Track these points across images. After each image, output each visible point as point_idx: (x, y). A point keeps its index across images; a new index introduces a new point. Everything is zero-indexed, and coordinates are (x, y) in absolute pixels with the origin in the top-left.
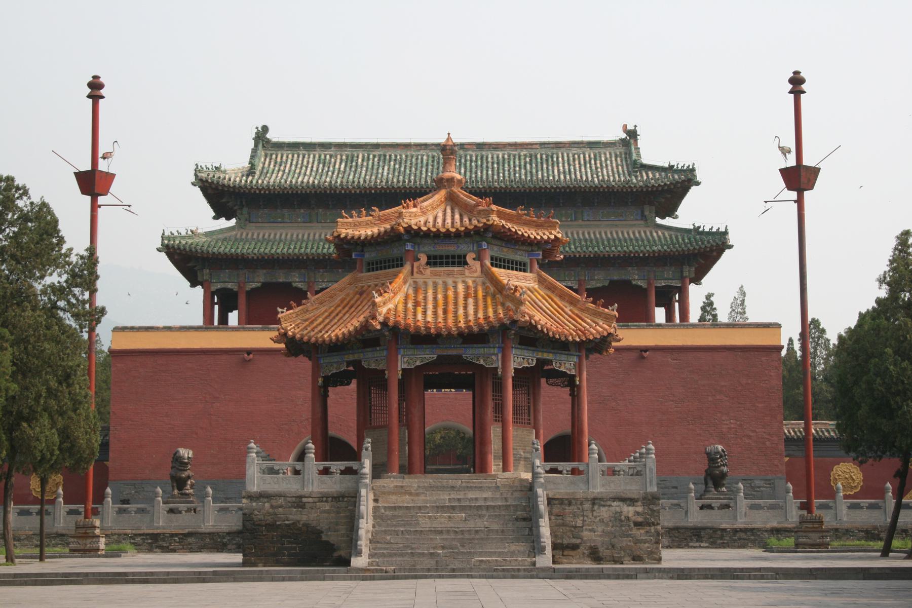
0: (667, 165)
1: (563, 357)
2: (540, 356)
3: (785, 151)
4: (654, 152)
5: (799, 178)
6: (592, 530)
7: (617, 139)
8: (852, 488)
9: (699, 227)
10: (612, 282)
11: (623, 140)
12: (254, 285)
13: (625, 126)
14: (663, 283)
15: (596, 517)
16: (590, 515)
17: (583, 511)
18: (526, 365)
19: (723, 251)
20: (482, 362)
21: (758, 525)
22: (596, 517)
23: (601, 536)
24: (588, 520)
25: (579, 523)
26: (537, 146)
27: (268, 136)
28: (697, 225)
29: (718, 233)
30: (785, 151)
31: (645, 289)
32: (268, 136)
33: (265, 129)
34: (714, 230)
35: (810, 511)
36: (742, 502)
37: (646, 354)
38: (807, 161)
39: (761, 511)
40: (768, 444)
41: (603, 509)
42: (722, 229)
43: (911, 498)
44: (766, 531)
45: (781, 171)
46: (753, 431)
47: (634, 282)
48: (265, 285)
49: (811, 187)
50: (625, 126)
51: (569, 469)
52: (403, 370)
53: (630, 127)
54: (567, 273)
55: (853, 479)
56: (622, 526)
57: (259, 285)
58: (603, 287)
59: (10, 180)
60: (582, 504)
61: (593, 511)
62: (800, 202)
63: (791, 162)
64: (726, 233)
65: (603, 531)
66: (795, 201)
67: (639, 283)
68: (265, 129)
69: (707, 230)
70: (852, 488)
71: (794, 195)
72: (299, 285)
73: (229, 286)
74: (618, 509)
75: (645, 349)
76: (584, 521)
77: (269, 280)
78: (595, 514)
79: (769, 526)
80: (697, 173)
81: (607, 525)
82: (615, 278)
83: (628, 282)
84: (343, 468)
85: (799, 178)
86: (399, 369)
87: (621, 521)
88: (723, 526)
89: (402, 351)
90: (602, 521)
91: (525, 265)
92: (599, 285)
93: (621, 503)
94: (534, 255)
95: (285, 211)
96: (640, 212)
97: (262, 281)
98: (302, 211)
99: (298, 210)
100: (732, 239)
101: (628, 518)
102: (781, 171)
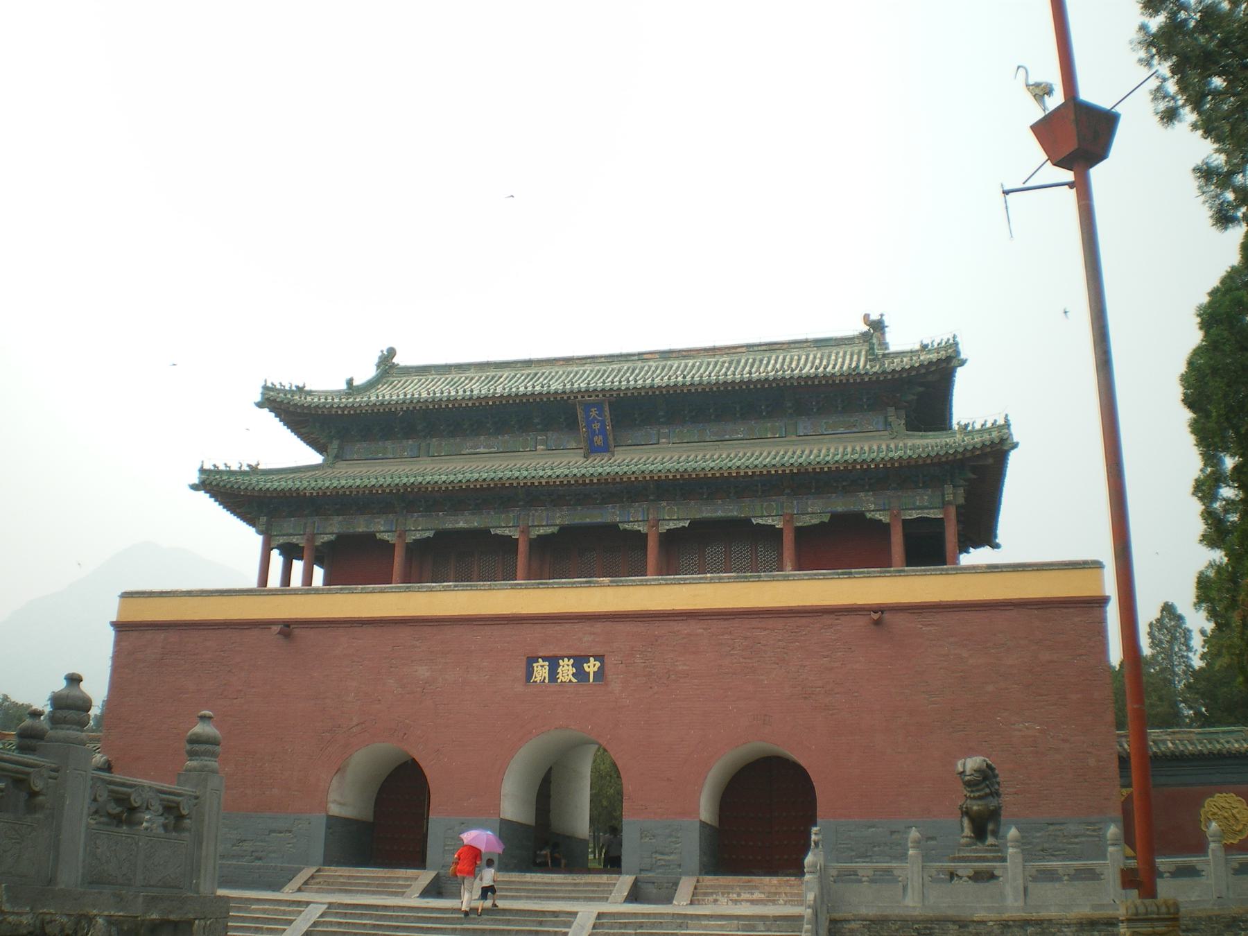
0: (917, 347)
3: (1041, 92)
4: (904, 338)
7: (856, 333)
8: (1235, 833)
9: (966, 426)
10: (835, 517)
11: (864, 335)
12: (326, 538)
13: (866, 317)
14: (915, 515)
21: (1052, 913)
26: (743, 350)
27: (395, 360)
28: (963, 423)
30: (1041, 92)
32: (395, 360)
33: (392, 352)
34: (989, 425)
35: (1149, 891)
36: (1013, 867)
37: (887, 616)
39: (1057, 885)
42: (1001, 422)
44: (1068, 925)
46: (1064, 741)
47: (869, 515)
48: (340, 537)
50: (866, 317)
53: (874, 317)
54: (765, 504)
55: (1236, 819)
57: (332, 537)
58: (822, 523)
62: (1082, 188)
63: (1056, 100)
64: (1007, 425)
66: (1071, 185)
67: (878, 516)
68: (392, 352)
70: (1235, 833)
71: (1069, 176)
72: (386, 537)
73: (294, 540)
75: (881, 609)
77: (344, 530)
80: (1013, 429)
82: (839, 509)
83: (861, 515)
84: (1236, 865)
88: (979, 916)
92: (815, 521)
95: (389, 444)
96: (881, 419)
97: (336, 531)
98: (410, 442)
99: (404, 442)
100: (1017, 434)
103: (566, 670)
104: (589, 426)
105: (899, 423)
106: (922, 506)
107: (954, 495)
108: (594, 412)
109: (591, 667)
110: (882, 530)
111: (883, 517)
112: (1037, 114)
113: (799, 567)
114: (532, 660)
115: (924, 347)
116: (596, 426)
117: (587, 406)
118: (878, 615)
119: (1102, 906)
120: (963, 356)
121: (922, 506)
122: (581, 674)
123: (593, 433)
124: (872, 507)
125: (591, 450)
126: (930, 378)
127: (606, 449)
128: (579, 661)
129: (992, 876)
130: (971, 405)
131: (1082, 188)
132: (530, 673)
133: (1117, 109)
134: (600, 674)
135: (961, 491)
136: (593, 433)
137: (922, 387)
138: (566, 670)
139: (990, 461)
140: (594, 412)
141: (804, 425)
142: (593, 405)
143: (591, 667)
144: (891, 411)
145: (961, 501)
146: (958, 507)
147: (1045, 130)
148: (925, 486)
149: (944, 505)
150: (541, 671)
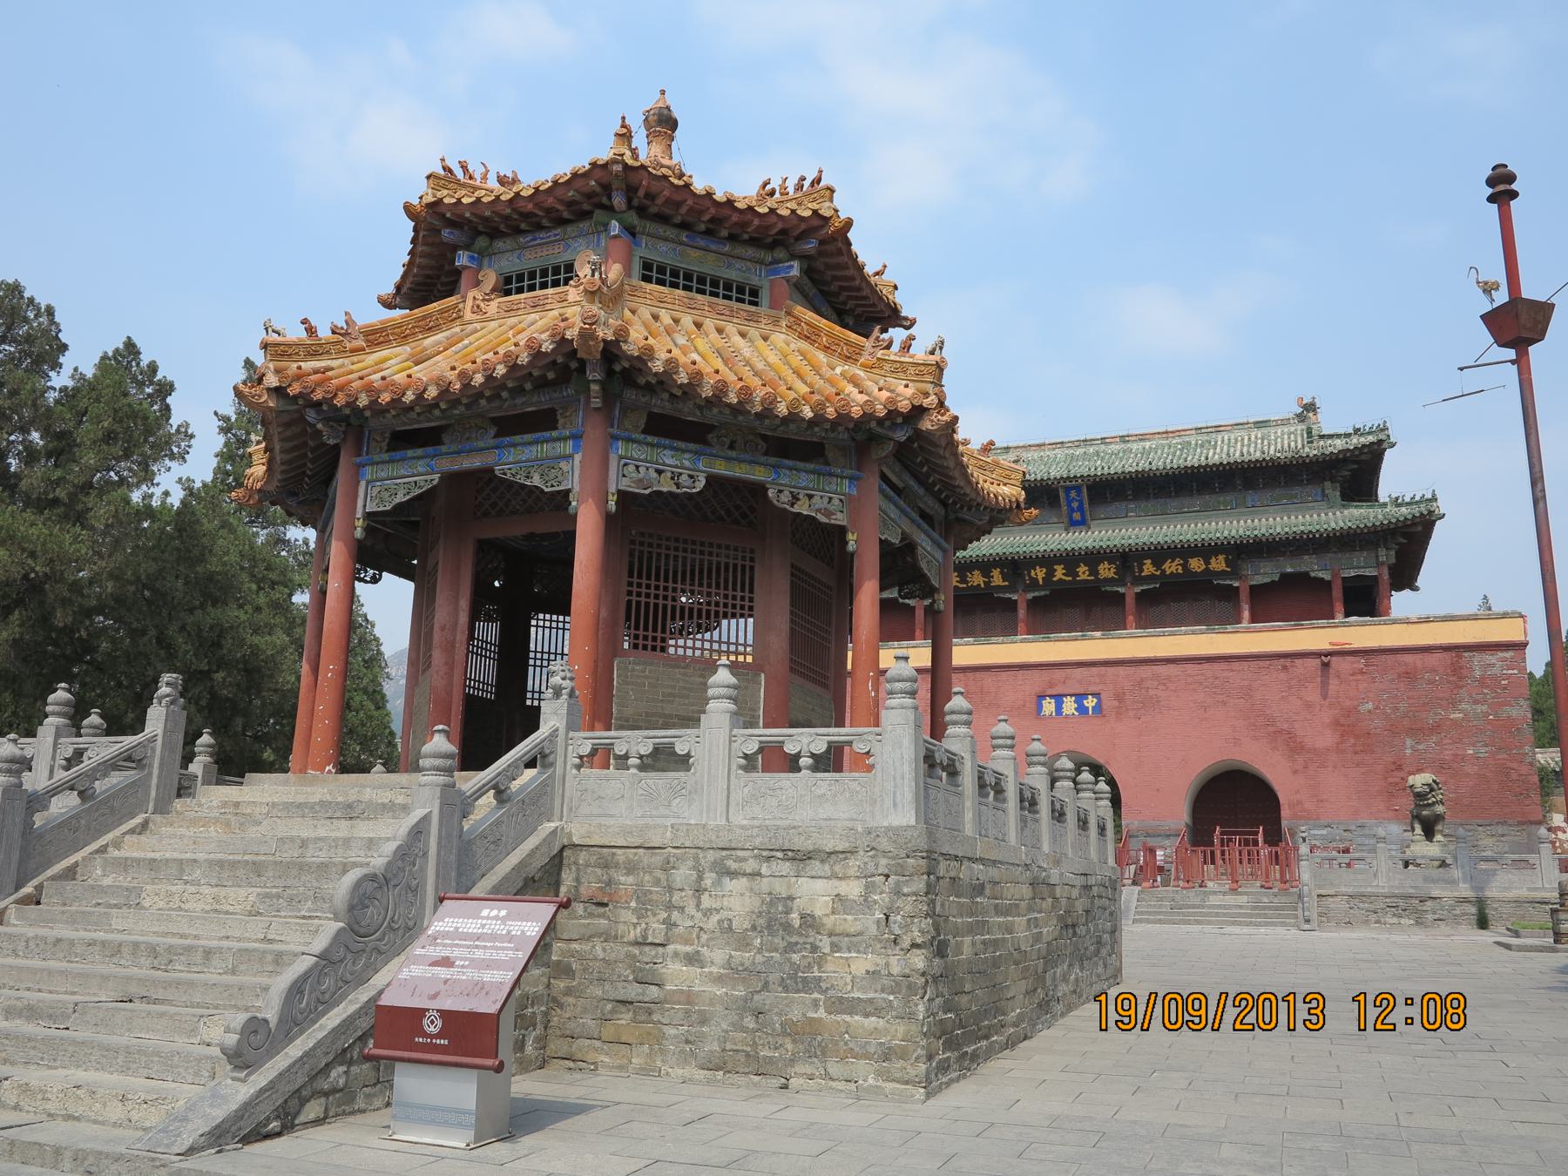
1: (805, 480)
2: (721, 469)
3: (1488, 289)
5: (1518, 325)
6: (693, 959)
10: (1284, 576)
15: (708, 913)
16: (691, 910)
17: (670, 889)
18: (666, 486)
19: (1433, 523)
20: (536, 481)
22: (708, 913)
23: (719, 980)
24: (684, 924)
25: (657, 930)
29: (1423, 500)
30: (1488, 289)
31: (1329, 583)
38: (1531, 290)
40: (1514, 776)
41: (730, 884)
43: (5, 539)
45: (1485, 318)
49: (1540, 336)
51: (646, 749)
52: (369, 516)
56: (791, 947)
59: (15, 289)
60: (667, 867)
61: (699, 891)
62: (1521, 362)
63: (1502, 297)
65: (728, 964)
66: (1513, 362)
69: (1407, 499)
71: (1511, 354)
74: (780, 888)
76: (670, 924)
78: (706, 902)
79: (1512, 894)
81: (744, 944)
85: (1518, 325)
86: (359, 514)
87: (787, 927)
89: (368, 472)
90: (727, 929)
91: (754, 293)
92: (1267, 580)
93: (786, 868)
94: (776, 272)
100: (1443, 506)
101: (809, 921)
102: (1485, 318)
103: (1069, 706)
104: (1069, 505)
105: (1335, 494)
106: (1359, 566)
107: (1387, 556)
108: (1073, 494)
109: (1090, 703)
110: (1325, 586)
111: (1326, 576)
112: (1488, 308)
113: (1253, 620)
114: (1042, 697)
115: (1357, 431)
116: (1075, 505)
117: (1068, 489)
118: (1325, 659)
119: (1536, 889)
120: (1392, 440)
121: (1359, 566)
122: (1082, 709)
123: (1073, 510)
124: (1317, 568)
125: (1073, 524)
126: (1363, 457)
127: (1082, 523)
128: (1080, 697)
129: (683, 762)
130: (1396, 481)
131: (1521, 362)
132: (1040, 707)
133: (1553, 300)
134: (1098, 708)
135: (1393, 553)
136: (1073, 510)
137: (1356, 470)
138: (1069, 706)
139: (1420, 528)
140: (1073, 494)
141: (1250, 497)
142: (1073, 488)
143: (1090, 703)
144: (1328, 484)
145: (1393, 560)
146: (1390, 568)
147: (1492, 320)
148: (1361, 549)
149: (1379, 565)
150: (1049, 706)
